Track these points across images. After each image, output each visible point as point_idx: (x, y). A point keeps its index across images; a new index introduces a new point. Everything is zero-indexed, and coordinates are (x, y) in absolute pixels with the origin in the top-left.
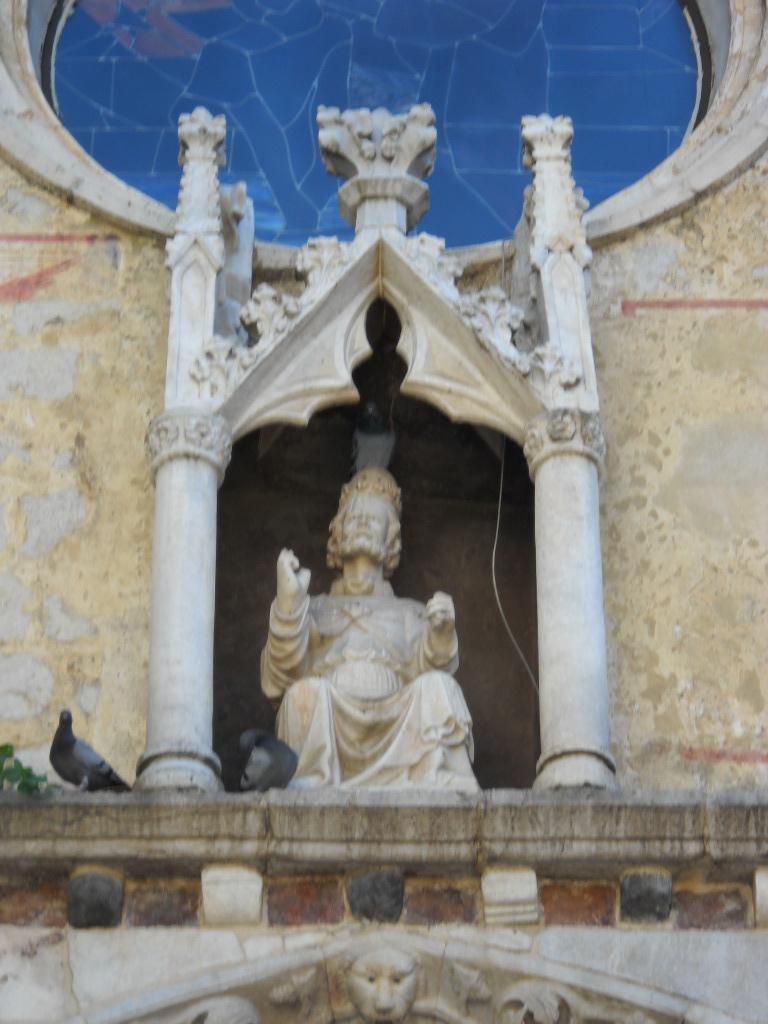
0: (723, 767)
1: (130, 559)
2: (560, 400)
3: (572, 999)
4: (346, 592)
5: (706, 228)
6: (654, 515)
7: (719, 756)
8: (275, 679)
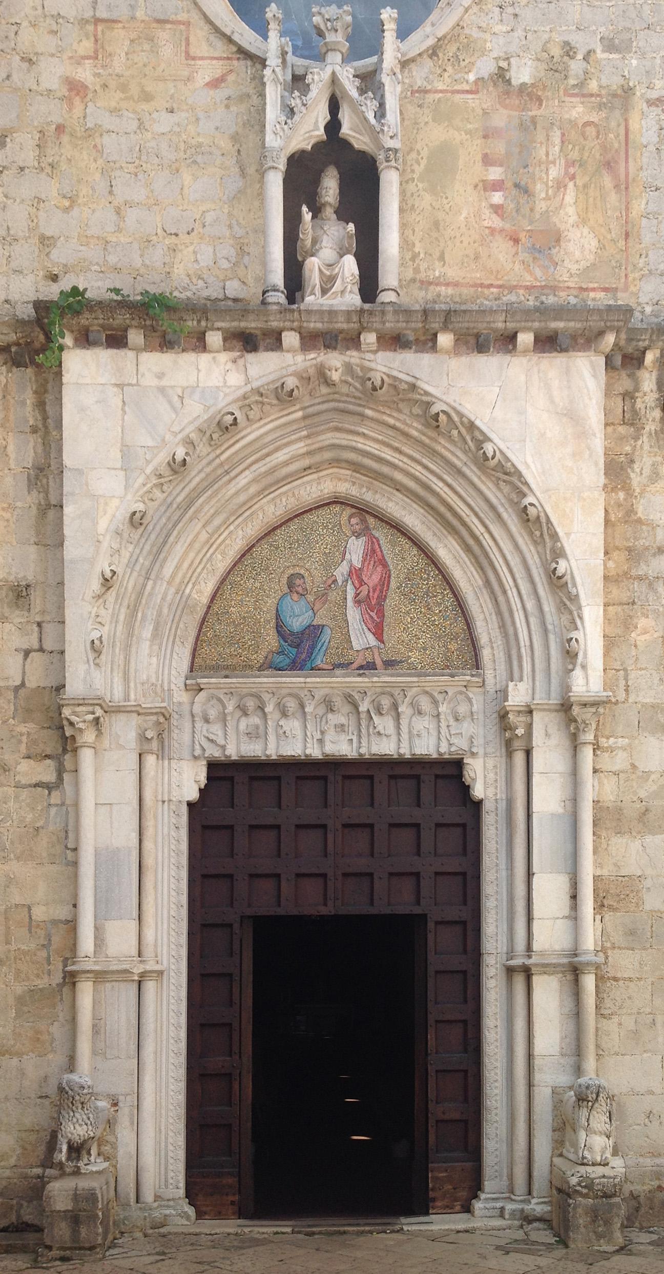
0: (432, 288)
1: (257, 203)
2: (390, 144)
3: (385, 378)
4: (323, 219)
5: (441, 55)
6: (417, 185)
7: (430, 283)
8: (301, 254)
